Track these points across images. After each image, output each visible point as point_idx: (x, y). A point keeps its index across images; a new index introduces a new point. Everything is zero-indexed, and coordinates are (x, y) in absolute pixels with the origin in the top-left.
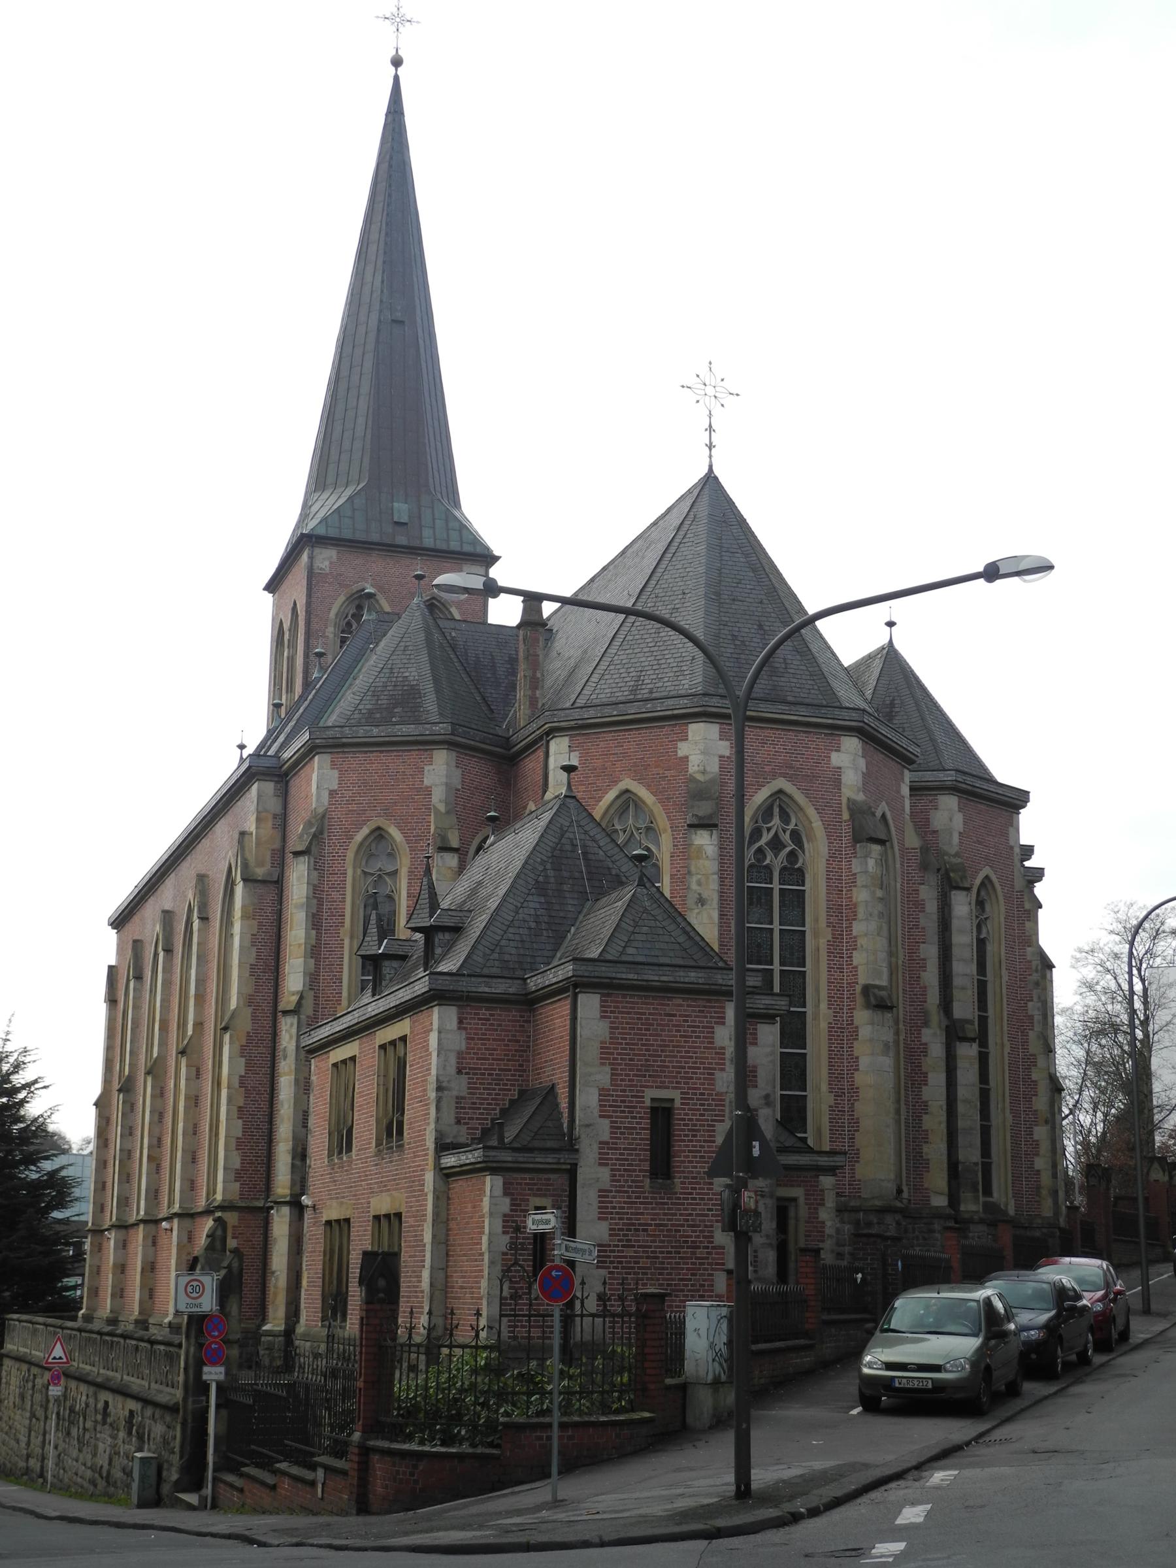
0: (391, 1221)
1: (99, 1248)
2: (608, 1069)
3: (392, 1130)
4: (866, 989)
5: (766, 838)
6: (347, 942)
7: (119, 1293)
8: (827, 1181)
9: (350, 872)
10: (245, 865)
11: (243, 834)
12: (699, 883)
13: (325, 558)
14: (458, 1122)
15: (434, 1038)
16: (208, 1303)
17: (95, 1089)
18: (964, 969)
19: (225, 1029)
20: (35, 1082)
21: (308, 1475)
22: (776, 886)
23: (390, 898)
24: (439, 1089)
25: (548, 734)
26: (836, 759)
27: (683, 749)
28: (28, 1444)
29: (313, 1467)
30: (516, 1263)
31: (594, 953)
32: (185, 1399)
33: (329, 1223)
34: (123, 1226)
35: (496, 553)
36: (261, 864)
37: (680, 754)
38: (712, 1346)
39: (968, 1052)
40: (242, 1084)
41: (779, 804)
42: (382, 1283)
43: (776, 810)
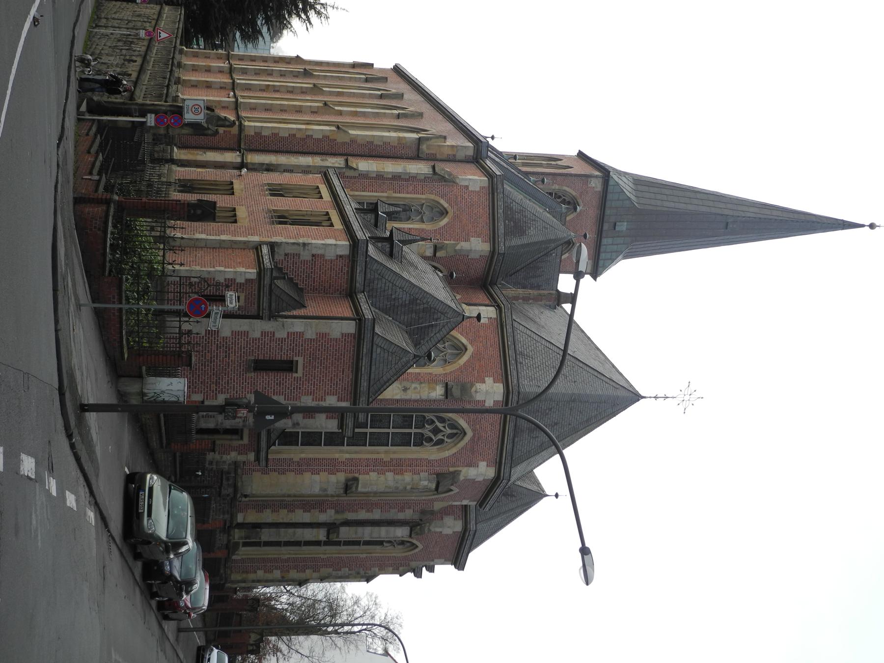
0: (232, 217)
1: (219, 57)
2: (314, 337)
3: (282, 218)
4: (356, 480)
5: (440, 425)
6: (385, 194)
7: (195, 69)
8: (251, 456)
9: (423, 196)
10: (428, 139)
11: (445, 138)
12: (415, 388)
13: (596, 185)
14: (286, 255)
15: (331, 242)
16: (189, 117)
17: (305, 56)
18: (367, 533)
19: (338, 127)
20: (310, 23)
21: (95, 171)
22: (413, 431)
23: (409, 219)
24: (304, 244)
25: (498, 306)
26: (483, 465)
27: (489, 380)
28: (114, 19)
29: (100, 174)
30: (209, 285)
31: (378, 330)
32: (137, 104)
33: (232, 183)
34: (231, 70)
35: (598, 279)
36: (428, 148)
37: (486, 379)
38: (163, 392)
39: (321, 535)
40: (308, 136)
41: (458, 433)
42: (199, 212)
43: (455, 431)
